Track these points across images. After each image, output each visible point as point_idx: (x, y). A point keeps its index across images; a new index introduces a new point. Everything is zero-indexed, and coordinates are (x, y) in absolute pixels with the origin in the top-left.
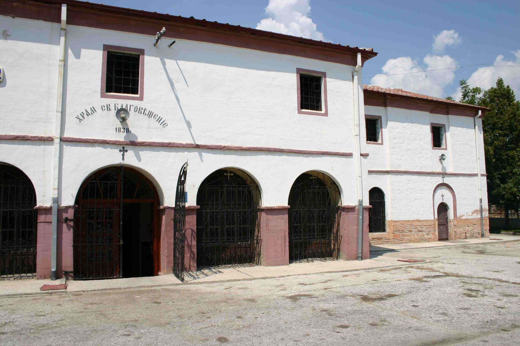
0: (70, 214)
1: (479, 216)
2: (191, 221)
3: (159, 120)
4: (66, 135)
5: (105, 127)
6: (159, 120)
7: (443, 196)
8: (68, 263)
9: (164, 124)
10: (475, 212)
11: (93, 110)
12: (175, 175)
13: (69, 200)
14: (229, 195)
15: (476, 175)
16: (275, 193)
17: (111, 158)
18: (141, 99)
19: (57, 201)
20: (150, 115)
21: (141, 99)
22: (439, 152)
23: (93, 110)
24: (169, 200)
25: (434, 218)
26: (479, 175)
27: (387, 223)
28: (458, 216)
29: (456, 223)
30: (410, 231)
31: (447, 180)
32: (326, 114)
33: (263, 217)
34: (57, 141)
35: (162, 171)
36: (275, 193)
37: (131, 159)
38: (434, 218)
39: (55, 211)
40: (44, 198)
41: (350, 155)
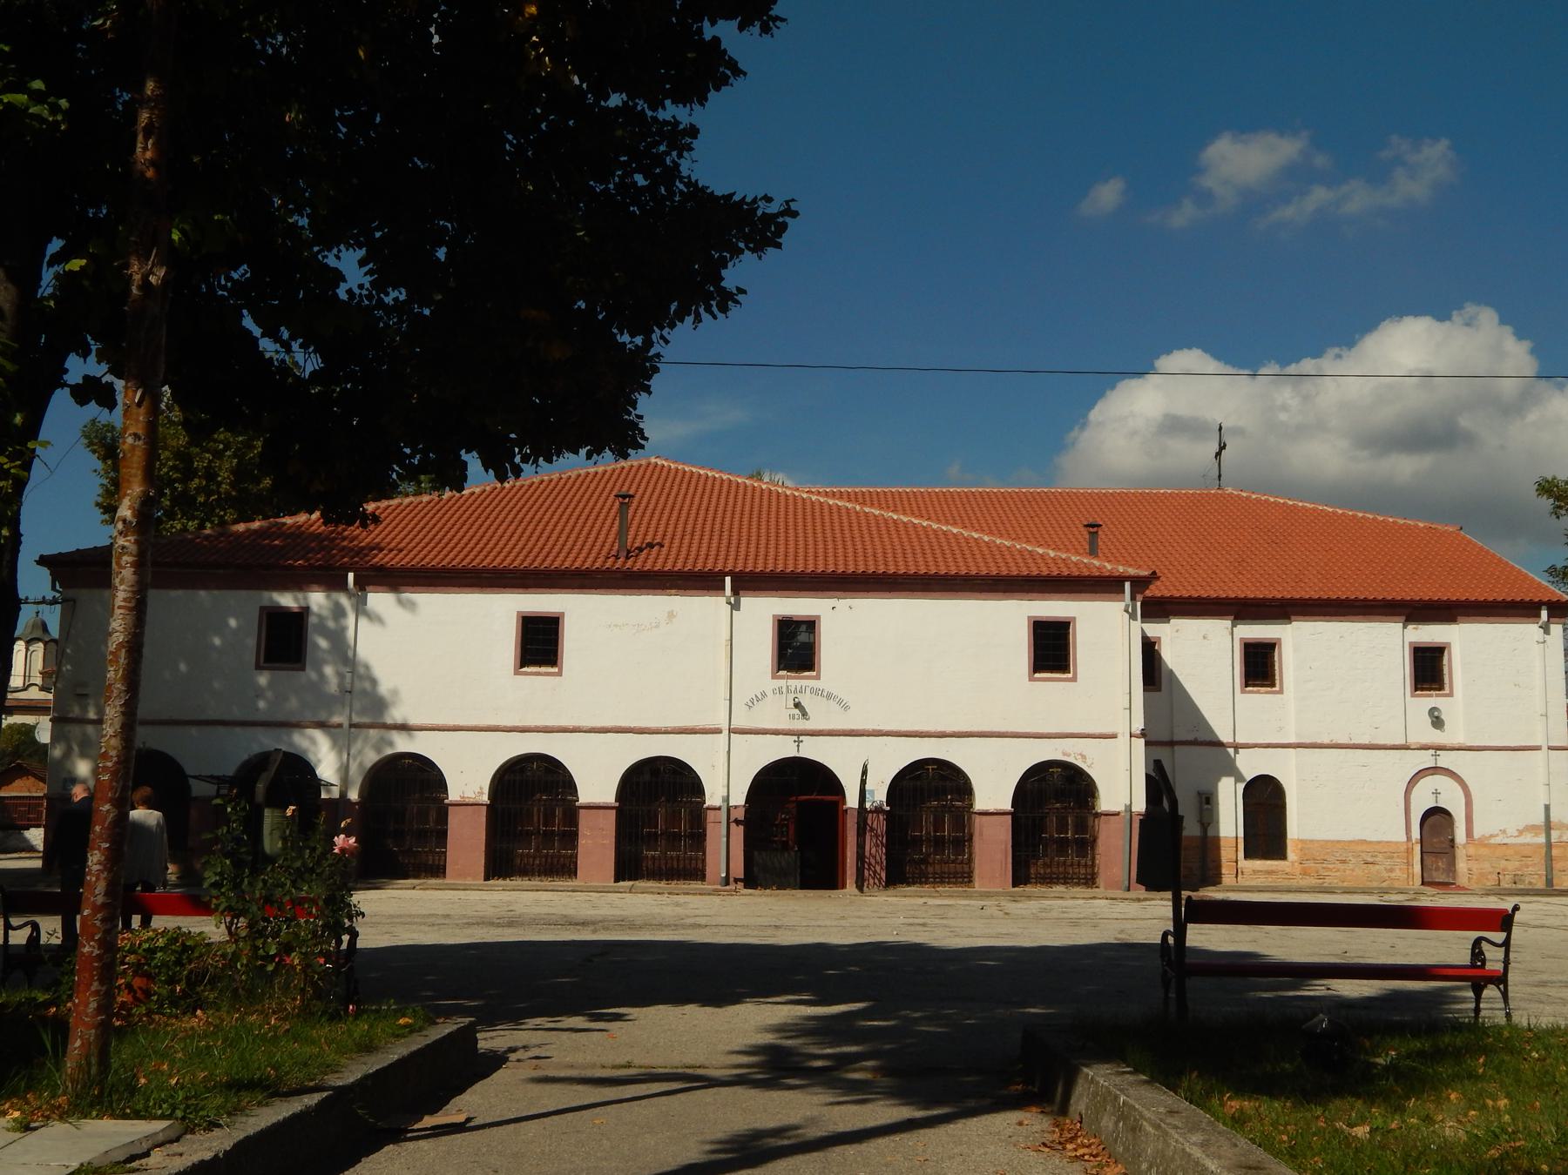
0: (740, 815)
1: (1542, 839)
2: (879, 824)
3: (840, 702)
4: (736, 724)
5: (776, 713)
6: (840, 702)
7: (1436, 793)
8: (738, 869)
9: (846, 708)
10: (1531, 828)
11: (764, 695)
12: (866, 771)
13: (739, 798)
14: (931, 789)
15: (1538, 748)
16: (993, 792)
17: (784, 749)
18: (818, 677)
19: (727, 799)
20: (829, 696)
21: (818, 677)
22: (1429, 701)
23: (764, 695)
24: (852, 801)
25: (1409, 838)
26: (1545, 748)
27: (1289, 843)
28: (1476, 836)
29: (1472, 850)
30: (1344, 862)
31: (1445, 760)
32: (1074, 679)
33: (977, 819)
34: (726, 732)
35: (842, 760)
36: (993, 792)
37: (812, 750)
38: (1409, 838)
39: (724, 810)
40: (713, 797)
41: (1114, 736)
